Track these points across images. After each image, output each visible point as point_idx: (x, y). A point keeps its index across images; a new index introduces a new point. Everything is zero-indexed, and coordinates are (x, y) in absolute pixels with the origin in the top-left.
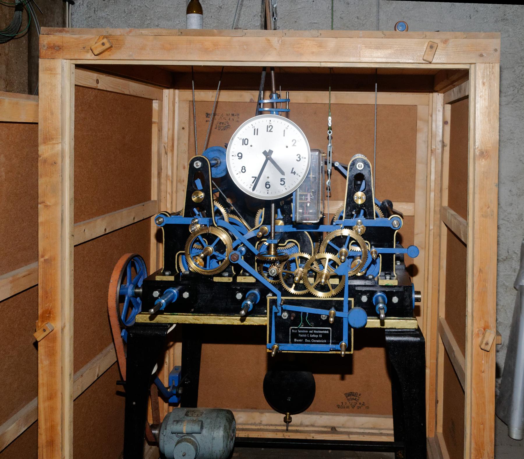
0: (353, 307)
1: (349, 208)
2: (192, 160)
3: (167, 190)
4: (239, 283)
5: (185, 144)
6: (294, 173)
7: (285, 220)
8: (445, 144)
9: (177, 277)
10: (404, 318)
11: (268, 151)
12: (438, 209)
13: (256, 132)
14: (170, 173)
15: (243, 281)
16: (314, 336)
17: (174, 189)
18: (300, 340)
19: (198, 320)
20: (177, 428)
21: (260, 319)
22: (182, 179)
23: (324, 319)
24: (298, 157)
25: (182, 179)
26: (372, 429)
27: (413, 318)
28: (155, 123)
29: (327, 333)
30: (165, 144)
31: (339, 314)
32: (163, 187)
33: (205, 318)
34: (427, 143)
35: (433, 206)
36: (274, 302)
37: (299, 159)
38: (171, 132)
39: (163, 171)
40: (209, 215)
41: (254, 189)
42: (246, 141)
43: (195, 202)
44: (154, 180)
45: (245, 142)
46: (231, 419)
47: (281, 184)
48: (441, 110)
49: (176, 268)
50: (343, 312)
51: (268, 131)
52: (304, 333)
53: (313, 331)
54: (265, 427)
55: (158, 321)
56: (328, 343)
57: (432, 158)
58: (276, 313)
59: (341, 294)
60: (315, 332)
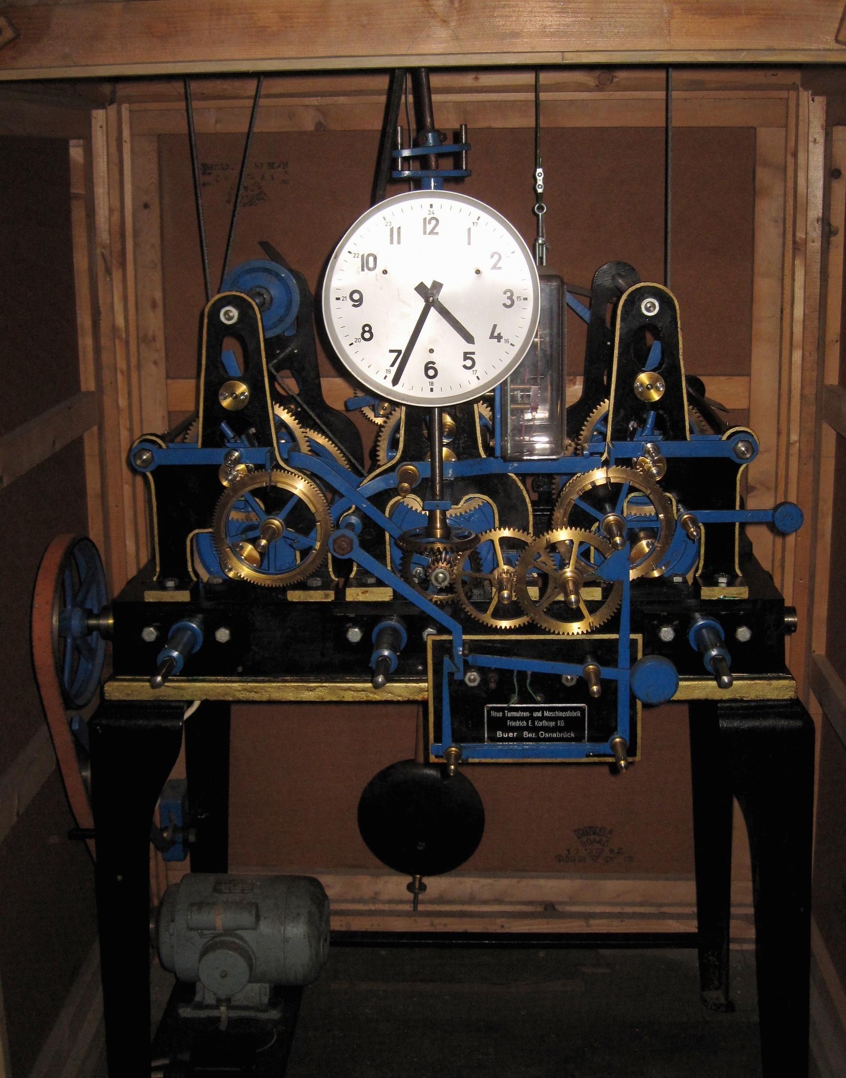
0: (640, 655)
1: (622, 412)
2: (214, 304)
3: (116, 363)
4: (350, 602)
5: (153, 246)
6: (499, 338)
7: (459, 447)
8: (833, 229)
9: (194, 593)
10: (764, 675)
11: (429, 285)
12: (811, 391)
13: (395, 235)
14: (120, 321)
15: (361, 598)
16: (545, 723)
17: (134, 361)
18: (511, 735)
19: (256, 692)
20: (201, 918)
21: (407, 687)
22: (150, 334)
23: (569, 684)
24: (508, 298)
25: (150, 334)
26: (641, 904)
27: (785, 675)
28: (77, 197)
29: (576, 717)
30: (104, 247)
31: (608, 673)
32: (105, 357)
33: (272, 687)
34: (781, 224)
35: (799, 385)
36: (443, 649)
37: (509, 302)
38: (116, 215)
39: (103, 316)
40: (263, 439)
41: (395, 381)
42: (371, 259)
43: (229, 409)
44: (86, 342)
45: (367, 263)
46: (319, 896)
47: (465, 367)
48: (821, 139)
49: (190, 569)
50: (616, 666)
51: (428, 232)
52: (521, 719)
53: (543, 713)
54: (387, 907)
55: (160, 696)
56: (579, 739)
57: (797, 262)
58: (451, 674)
59: (611, 625)
60: (546, 714)
